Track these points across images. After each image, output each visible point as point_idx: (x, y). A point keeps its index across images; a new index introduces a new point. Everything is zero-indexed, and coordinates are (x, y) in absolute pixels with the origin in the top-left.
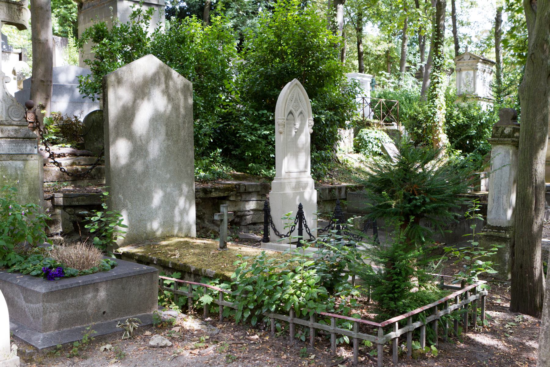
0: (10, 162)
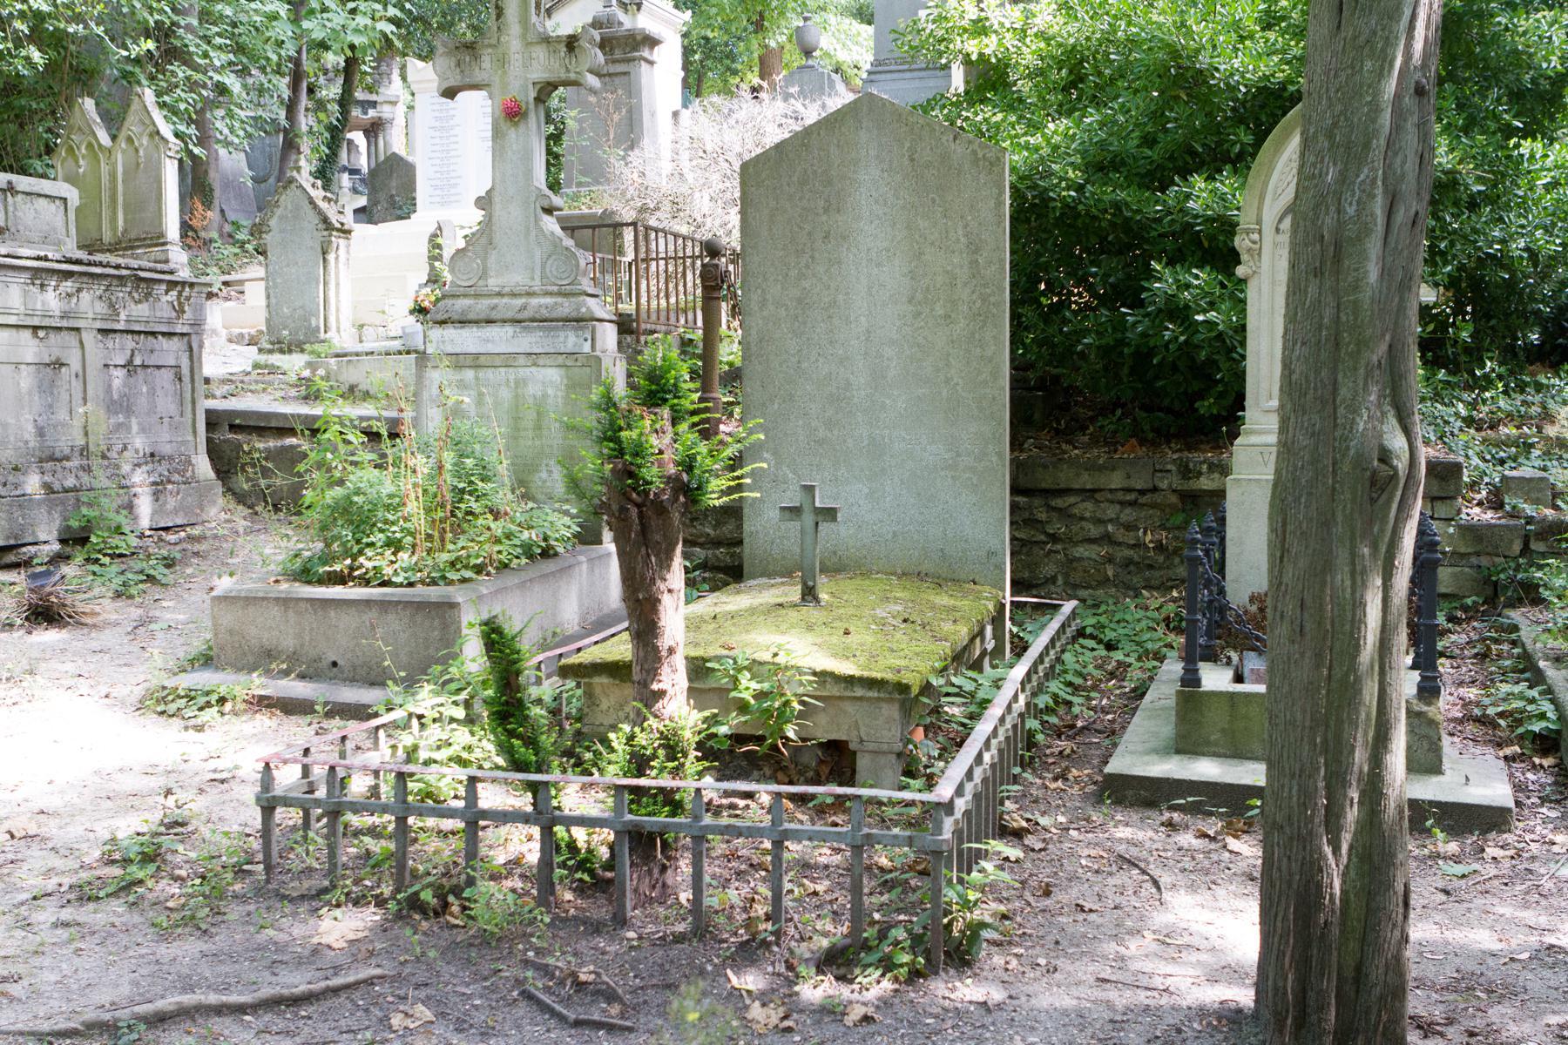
0: (533, 369)
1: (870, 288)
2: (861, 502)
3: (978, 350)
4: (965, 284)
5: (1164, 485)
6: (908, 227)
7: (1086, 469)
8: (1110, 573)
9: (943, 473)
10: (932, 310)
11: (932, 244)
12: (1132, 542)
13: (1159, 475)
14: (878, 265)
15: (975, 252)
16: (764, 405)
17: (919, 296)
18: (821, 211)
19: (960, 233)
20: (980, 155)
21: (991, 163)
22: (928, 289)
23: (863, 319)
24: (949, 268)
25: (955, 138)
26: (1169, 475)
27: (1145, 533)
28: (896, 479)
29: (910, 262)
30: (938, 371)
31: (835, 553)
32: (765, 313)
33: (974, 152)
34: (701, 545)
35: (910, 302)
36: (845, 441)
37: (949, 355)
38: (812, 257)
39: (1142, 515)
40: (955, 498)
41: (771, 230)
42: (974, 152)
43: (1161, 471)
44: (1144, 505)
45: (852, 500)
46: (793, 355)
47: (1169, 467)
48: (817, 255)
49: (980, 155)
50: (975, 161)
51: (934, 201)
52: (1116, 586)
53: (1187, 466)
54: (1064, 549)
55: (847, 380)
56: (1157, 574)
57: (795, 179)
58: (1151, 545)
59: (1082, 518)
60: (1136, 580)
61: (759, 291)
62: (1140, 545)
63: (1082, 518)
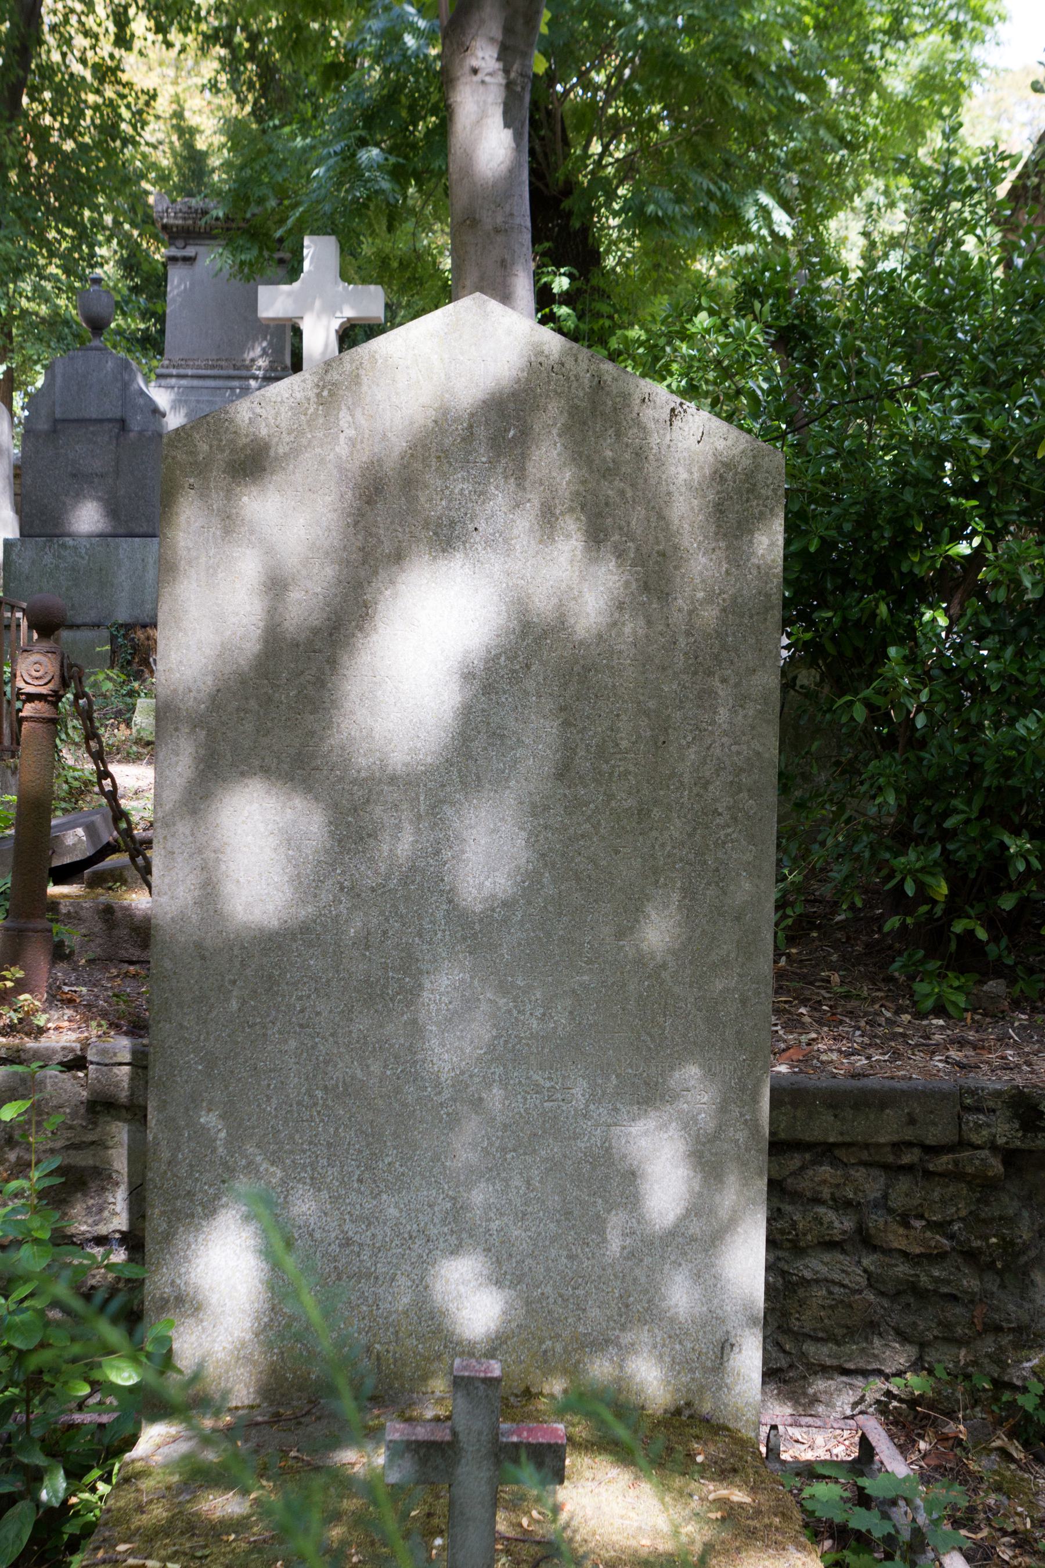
10: (611, 797)
12: (918, 1250)
24: (652, 704)
36: (397, 1091)
39: (936, 1195)
44: (933, 1174)
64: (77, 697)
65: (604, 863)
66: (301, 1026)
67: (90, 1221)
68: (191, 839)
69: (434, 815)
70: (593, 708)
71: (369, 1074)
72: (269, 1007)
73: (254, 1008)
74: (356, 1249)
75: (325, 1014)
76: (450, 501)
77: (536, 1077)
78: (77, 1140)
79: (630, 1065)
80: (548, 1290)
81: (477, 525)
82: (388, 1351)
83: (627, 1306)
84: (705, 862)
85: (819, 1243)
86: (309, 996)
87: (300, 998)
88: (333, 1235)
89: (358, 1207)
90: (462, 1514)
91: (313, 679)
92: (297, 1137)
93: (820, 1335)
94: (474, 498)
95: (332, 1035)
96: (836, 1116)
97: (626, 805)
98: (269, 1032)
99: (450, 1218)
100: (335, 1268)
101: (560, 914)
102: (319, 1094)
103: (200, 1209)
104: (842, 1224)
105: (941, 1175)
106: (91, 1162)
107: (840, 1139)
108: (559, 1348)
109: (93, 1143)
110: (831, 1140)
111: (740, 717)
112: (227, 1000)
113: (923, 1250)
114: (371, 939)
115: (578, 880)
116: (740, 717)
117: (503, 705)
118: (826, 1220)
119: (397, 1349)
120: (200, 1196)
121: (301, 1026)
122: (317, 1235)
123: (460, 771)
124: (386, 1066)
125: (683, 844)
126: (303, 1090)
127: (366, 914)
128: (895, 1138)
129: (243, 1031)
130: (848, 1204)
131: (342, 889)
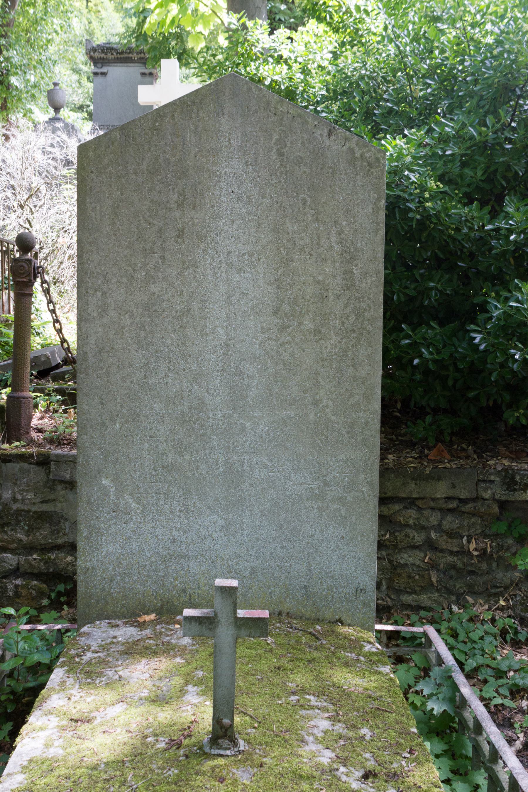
1: (229, 296)
2: (215, 535)
3: (351, 369)
4: (338, 297)
5: (487, 495)
6: (275, 230)
7: (413, 479)
8: (434, 579)
9: (308, 504)
10: (301, 324)
11: (302, 250)
12: (456, 549)
13: (483, 485)
14: (239, 271)
15: (350, 262)
16: (103, 424)
17: (286, 308)
18: (174, 206)
19: (333, 239)
20: (358, 155)
21: (369, 164)
22: (296, 300)
23: (221, 331)
24: (320, 278)
25: (330, 134)
26: (492, 486)
27: (469, 542)
28: (256, 511)
29: (276, 269)
30: (305, 391)
31: (184, 591)
32: (105, 320)
33: (351, 150)
34: (13, 551)
35: (275, 314)
36: (198, 467)
37: (317, 374)
38: (163, 258)
39: (466, 522)
40: (322, 531)
41: (114, 224)
42: (351, 150)
43: (484, 481)
44: (464, 512)
45: (205, 533)
46: (139, 369)
47: (492, 478)
48: (168, 256)
49: (358, 155)
50: (352, 161)
51: (304, 202)
52: (438, 591)
53: (513, 478)
54: (388, 555)
55: (201, 399)
56: (480, 580)
57: (144, 167)
58: (476, 553)
59: (407, 525)
60: (459, 585)
61: (99, 294)
62: (464, 552)
63: (407, 525)
64: (42, 283)
65: (298, 356)
66: (150, 437)
67: (53, 537)
68: (95, 346)
69: (214, 333)
70: (291, 280)
71: (184, 460)
72: (134, 428)
73: (127, 428)
74: (179, 544)
75: (162, 431)
76: (220, 177)
77: (265, 461)
78: (47, 499)
79: (311, 455)
80: (272, 563)
81: (233, 190)
82: (194, 593)
83: (310, 571)
84: (347, 356)
85: (407, 547)
86: (154, 422)
87: (149, 423)
88: (167, 537)
89: (179, 524)
90: (220, 651)
91: (153, 267)
92: (149, 490)
93: (408, 590)
94: (231, 176)
95: (165, 441)
96: (416, 484)
97: (308, 327)
98: (135, 440)
99: (224, 529)
100: (169, 553)
101: (276, 381)
102: (160, 469)
103: (103, 525)
104: (419, 538)
105: (468, 513)
106: (53, 509)
107: (417, 496)
108: (277, 591)
109: (54, 500)
110: (414, 496)
111: (364, 284)
112: (115, 424)
113: (459, 549)
114: (184, 394)
115: (284, 364)
116: (364, 284)
117: (247, 279)
118: (411, 535)
119: (200, 592)
120: (103, 519)
121: (150, 437)
122: (160, 537)
123: (226, 311)
124: (192, 456)
125: (336, 346)
126: (152, 468)
127: (181, 382)
128: (445, 495)
129: (122, 439)
130: (423, 528)
131: (169, 369)
